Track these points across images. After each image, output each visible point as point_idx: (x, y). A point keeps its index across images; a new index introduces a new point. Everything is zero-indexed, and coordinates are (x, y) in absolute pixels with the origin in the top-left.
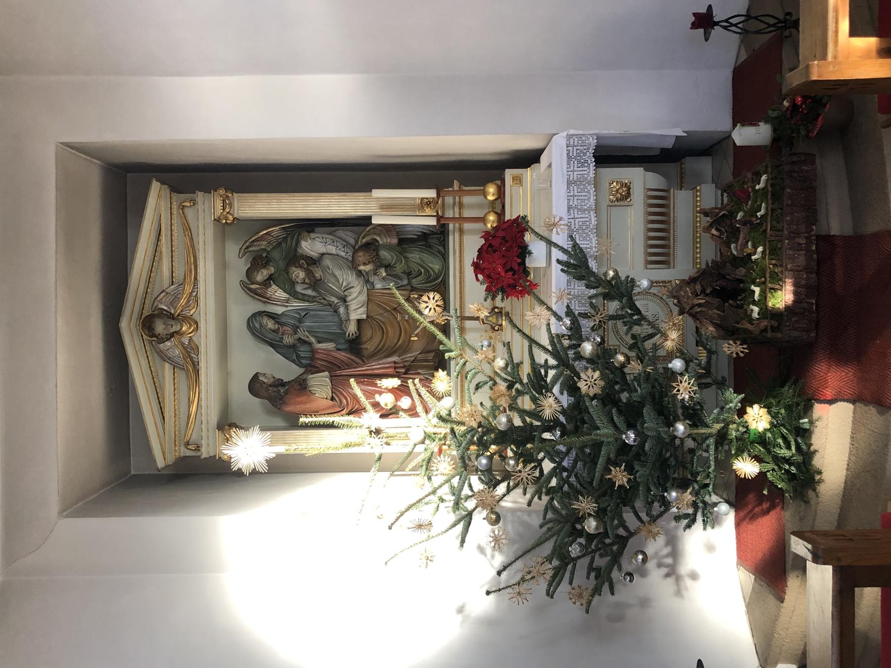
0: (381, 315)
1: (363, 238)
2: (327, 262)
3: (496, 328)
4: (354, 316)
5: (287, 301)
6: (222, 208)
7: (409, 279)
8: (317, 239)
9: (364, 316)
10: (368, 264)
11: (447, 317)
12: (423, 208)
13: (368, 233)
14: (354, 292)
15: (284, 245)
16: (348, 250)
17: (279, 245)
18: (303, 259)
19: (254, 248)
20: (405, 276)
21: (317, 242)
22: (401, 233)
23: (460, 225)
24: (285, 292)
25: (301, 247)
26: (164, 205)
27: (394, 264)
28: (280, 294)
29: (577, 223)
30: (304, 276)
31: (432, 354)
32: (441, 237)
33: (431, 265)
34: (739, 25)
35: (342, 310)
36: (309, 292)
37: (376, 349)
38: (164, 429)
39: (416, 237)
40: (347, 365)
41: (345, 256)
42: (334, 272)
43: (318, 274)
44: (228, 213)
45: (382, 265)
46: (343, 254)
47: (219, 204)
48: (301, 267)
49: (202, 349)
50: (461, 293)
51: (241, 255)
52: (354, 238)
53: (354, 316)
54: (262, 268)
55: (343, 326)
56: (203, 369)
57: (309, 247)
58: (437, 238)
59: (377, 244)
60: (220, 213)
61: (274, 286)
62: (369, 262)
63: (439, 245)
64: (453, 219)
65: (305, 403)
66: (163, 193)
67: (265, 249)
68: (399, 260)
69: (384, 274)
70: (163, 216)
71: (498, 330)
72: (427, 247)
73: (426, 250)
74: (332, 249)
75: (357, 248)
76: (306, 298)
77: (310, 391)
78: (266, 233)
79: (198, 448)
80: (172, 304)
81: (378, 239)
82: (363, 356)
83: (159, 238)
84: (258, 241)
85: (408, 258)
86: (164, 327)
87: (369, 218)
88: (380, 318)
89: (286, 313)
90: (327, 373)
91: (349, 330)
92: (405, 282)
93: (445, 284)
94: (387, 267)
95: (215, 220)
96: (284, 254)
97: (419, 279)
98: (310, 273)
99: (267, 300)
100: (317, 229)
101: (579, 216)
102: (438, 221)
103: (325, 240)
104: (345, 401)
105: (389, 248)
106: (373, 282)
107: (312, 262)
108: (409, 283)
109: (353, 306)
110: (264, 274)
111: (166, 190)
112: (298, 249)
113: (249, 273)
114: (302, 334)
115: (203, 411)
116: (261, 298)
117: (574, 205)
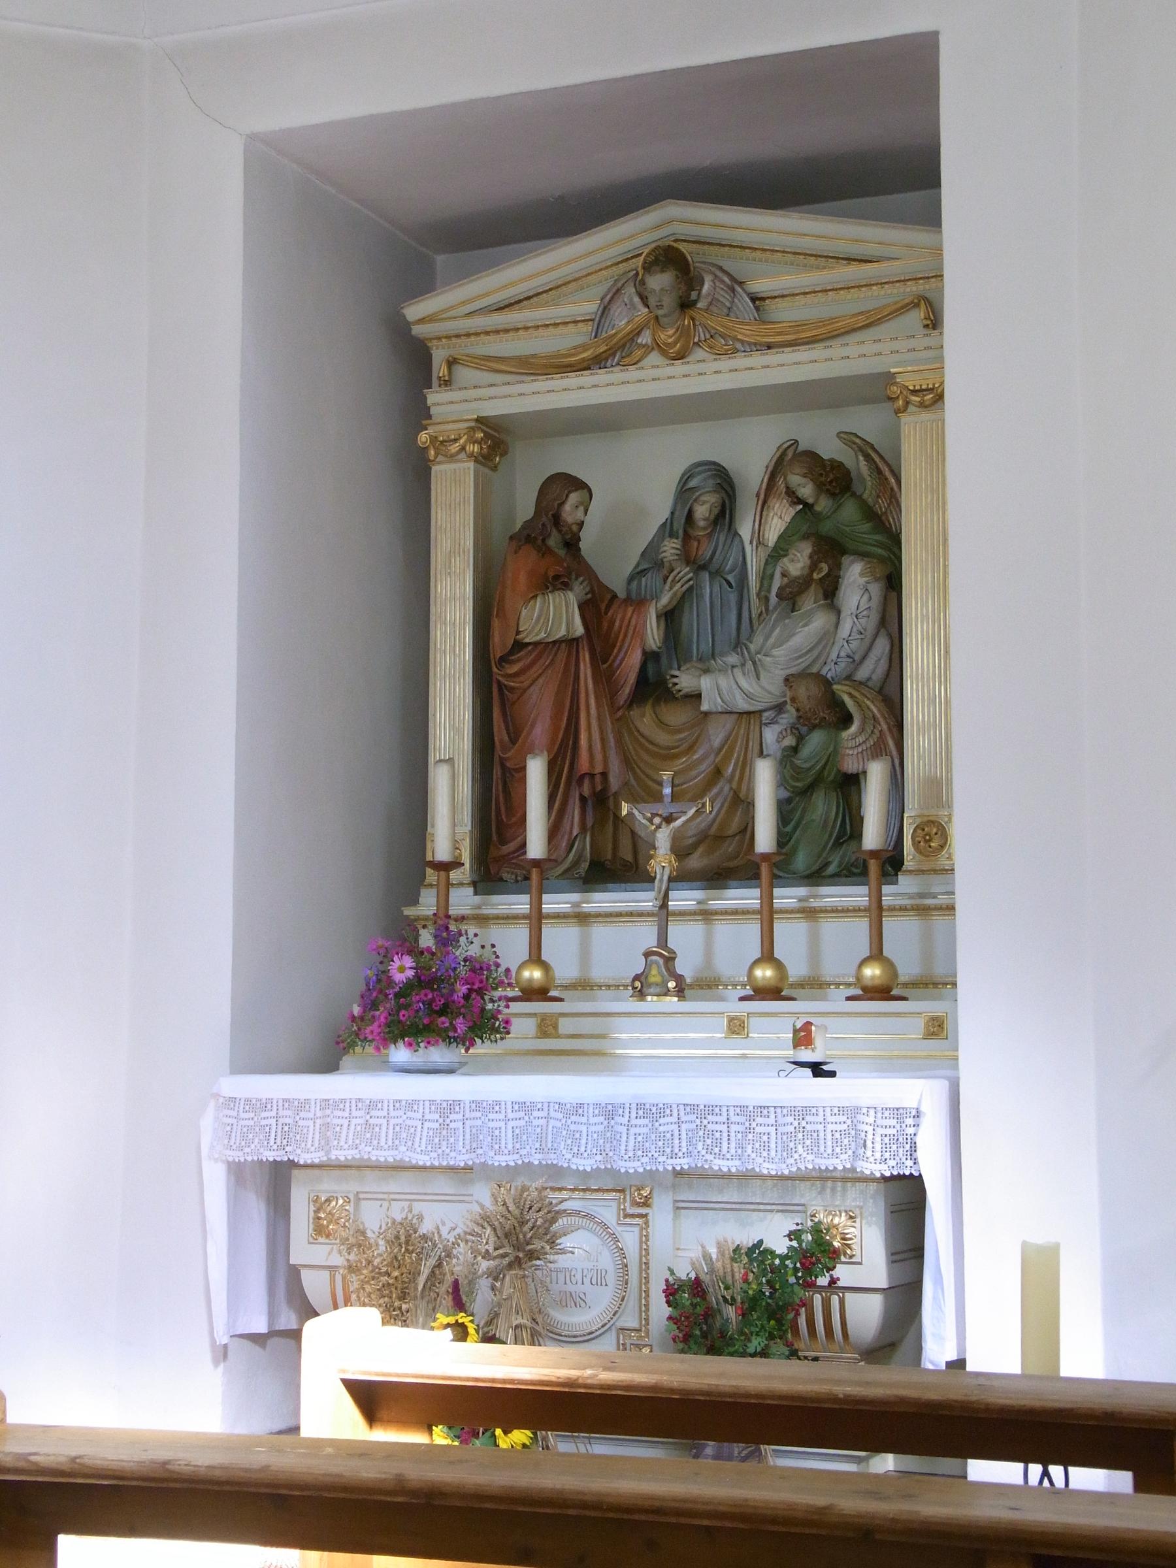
1: (850, 694)
2: (820, 621)
4: (706, 684)
5: (760, 543)
6: (918, 388)
8: (866, 597)
9: (705, 707)
16: (842, 665)
18: (830, 570)
25: (852, 562)
28: (775, 527)
29: (718, 1127)
31: (629, 857)
34: (1046, 1481)
35: (733, 659)
37: (643, 736)
38: (471, 314)
41: (829, 660)
48: (813, 567)
49: (632, 374)
52: (869, 679)
53: (706, 684)
60: (907, 384)
61: (792, 512)
63: (839, 866)
70: (897, 263)
77: (535, 597)
79: (446, 383)
81: (854, 728)
83: (854, 260)
89: (737, 540)
90: (579, 629)
101: (733, 1134)
103: (865, 613)
107: (830, 591)
109: (724, 682)
117: (754, 1125)
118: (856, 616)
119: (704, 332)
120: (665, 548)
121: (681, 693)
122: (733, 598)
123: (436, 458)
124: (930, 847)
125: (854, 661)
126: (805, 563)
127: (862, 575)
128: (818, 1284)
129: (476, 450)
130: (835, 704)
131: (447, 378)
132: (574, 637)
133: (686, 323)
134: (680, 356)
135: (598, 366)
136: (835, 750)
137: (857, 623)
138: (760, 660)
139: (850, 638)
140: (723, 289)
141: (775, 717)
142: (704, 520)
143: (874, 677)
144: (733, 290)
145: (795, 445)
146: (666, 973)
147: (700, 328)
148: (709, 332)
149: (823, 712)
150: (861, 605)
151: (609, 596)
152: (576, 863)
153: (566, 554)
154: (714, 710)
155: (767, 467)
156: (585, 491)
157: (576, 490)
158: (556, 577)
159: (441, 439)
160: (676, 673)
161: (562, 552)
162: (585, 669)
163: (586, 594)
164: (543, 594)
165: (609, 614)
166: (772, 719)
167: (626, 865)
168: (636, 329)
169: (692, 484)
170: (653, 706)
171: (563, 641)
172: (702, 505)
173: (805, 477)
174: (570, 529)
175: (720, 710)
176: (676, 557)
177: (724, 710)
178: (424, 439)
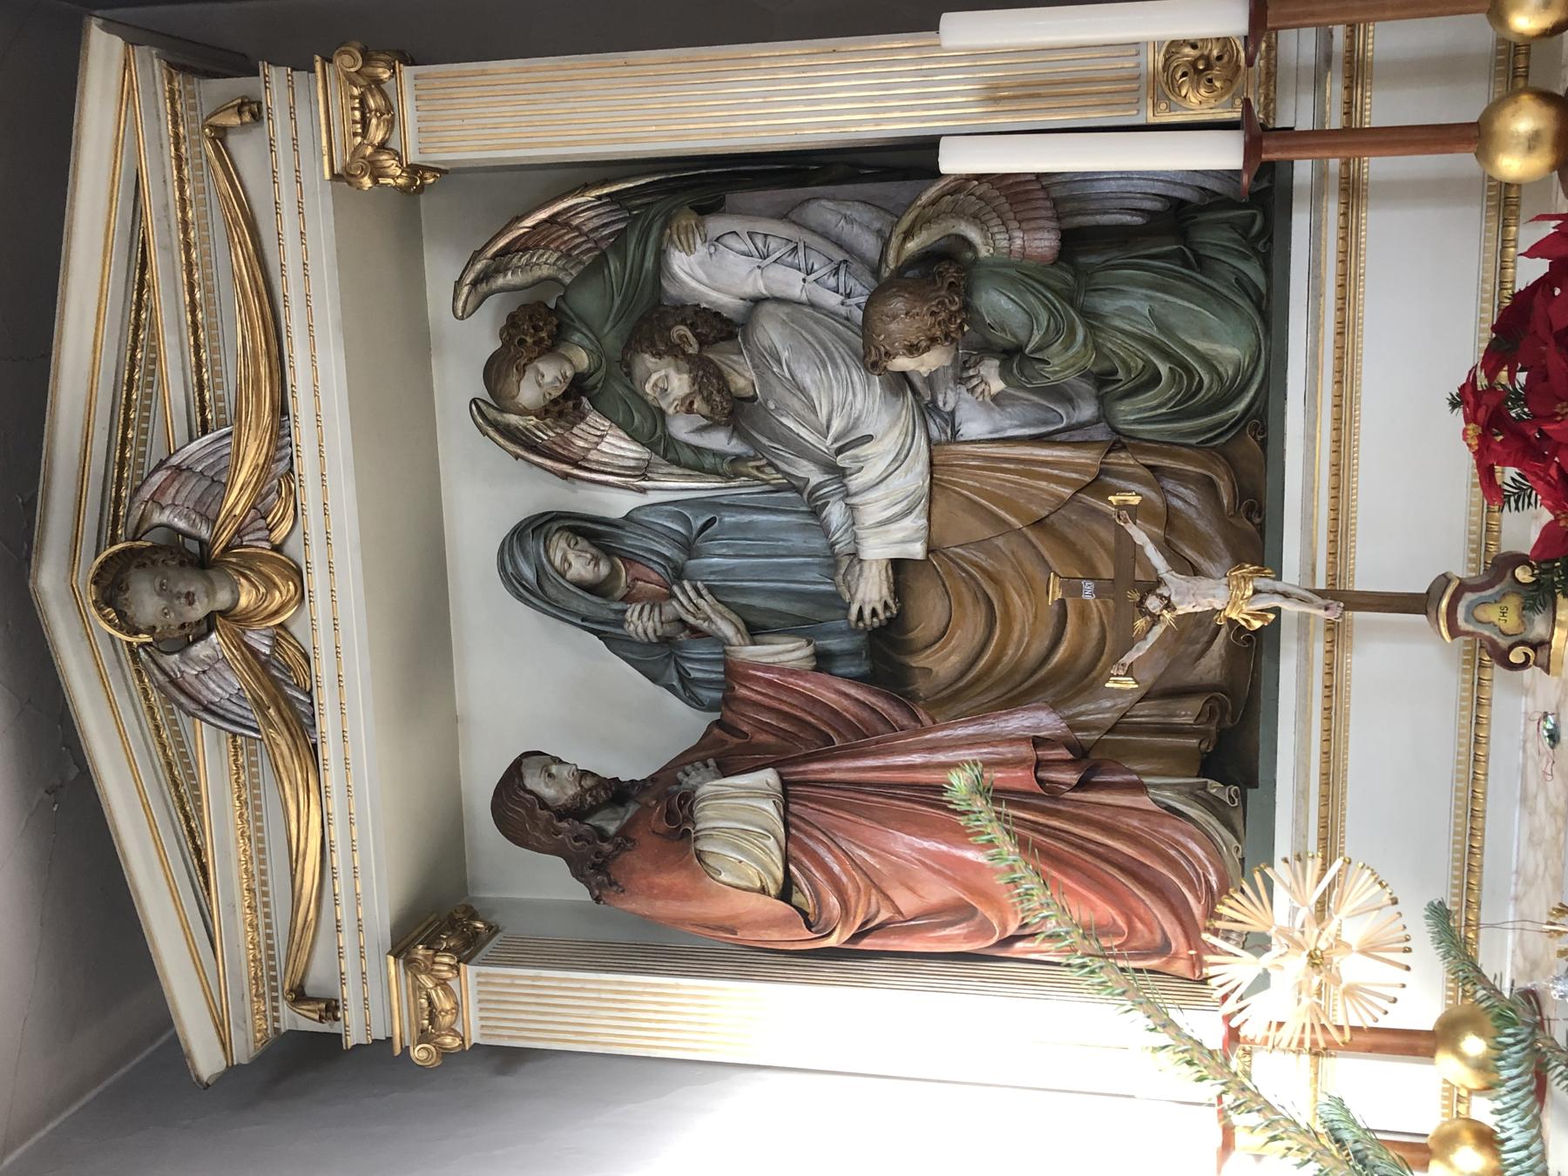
0: (979, 544)
1: (908, 235)
2: (771, 332)
3: (1516, 657)
4: (878, 549)
5: (643, 472)
7: (1101, 400)
8: (730, 241)
9: (917, 550)
10: (928, 349)
11: (1276, 602)
12: (1174, 87)
13: (930, 211)
14: (875, 460)
15: (614, 265)
16: (852, 283)
17: (600, 263)
18: (683, 322)
19: (509, 279)
20: (1087, 387)
21: (731, 256)
22: (1069, 206)
23: (1346, 164)
24: (634, 437)
26: (154, 129)
27: (1039, 349)
28: (618, 447)
30: (686, 390)
32: (1254, 217)
33: (1202, 346)
35: (835, 513)
36: (719, 441)
37: (963, 675)
39: (1138, 220)
40: (859, 734)
41: (843, 310)
42: (799, 375)
43: (743, 378)
44: (382, 147)
45: (987, 349)
46: (832, 300)
47: (344, 112)
48: (674, 350)
49: (323, 668)
50: (1337, 469)
51: (460, 304)
52: (879, 232)
53: (878, 549)
54: (540, 355)
55: (839, 578)
56: (330, 738)
57: (701, 274)
58: (1231, 223)
59: (969, 255)
61: (594, 418)
62: (933, 341)
63: (1246, 258)
64: (1320, 138)
65: (684, 896)
66: (138, 74)
67: (555, 279)
68: (1060, 331)
69: (997, 385)
71: (1524, 665)
72: (1187, 265)
73: (1184, 278)
74: (790, 283)
75: (886, 273)
76: (708, 462)
77: (699, 855)
78: (551, 220)
79: (331, 1008)
80: (206, 510)
81: (974, 235)
82: (913, 697)
84: (526, 250)
85: (1098, 316)
86: (163, 603)
87: (930, 145)
88: (981, 559)
89: (641, 516)
90: (767, 778)
91: (859, 596)
92: (1087, 411)
93: (1264, 430)
94: (1012, 357)
95: (335, 177)
96: (617, 301)
97: (1148, 400)
98: (708, 378)
99: (573, 465)
100: (735, 198)
102: (1252, 149)
104: (833, 901)
105: (1020, 274)
106: (952, 413)
108: (1104, 416)
109: (874, 508)
110: (548, 379)
111: (151, 68)
112: (664, 283)
113: (497, 372)
114: (688, 602)
115: (340, 886)
116: (548, 463)
118: (764, 257)
119: (254, 531)
120: (640, 630)
121: (891, 602)
122: (729, 519)
123: (457, 1034)
124: (1219, 58)
125: (845, 261)
126: (669, 365)
127: (690, 250)
128: (1249, 790)
129: (446, 960)
130: (930, 259)
131: (323, 1006)
132: (779, 789)
133: (234, 560)
134: (296, 574)
135: (311, 730)
136: (1015, 266)
137: (777, 255)
138: (836, 440)
139: (803, 265)
140: (177, 492)
141: (942, 417)
142: (597, 564)
143: (877, 225)
144: (178, 469)
145: (480, 403)
146: (1497, 588)
147: (247, 538)
148: (253, 520)
149: (940, 289)
150: (743, 248)
151: (716, 731)
152: (1213, 806)
153: (637, 802)
154: (924, 533)
155: (517, 457)
156: (525, 761)
157: (521, 777)
158: (670, 816)
159: (426, 1022)
160: (854, 610)
161: (633, 808)
162: (840, 770)
163: (707, 766)
164: (696, 839)
165: (745, 729)
166: (946, 421)
167: (1212, 711)
168: (242, 653)
169: (529, 573)
170: (914, 652)
171: (786, 808)
172: (570, 565)
173: (525, 371)
174: (590, 789)
175: (924, 522)
176: (657, 610)
177: (924, 514)
178: (423, 1055)
